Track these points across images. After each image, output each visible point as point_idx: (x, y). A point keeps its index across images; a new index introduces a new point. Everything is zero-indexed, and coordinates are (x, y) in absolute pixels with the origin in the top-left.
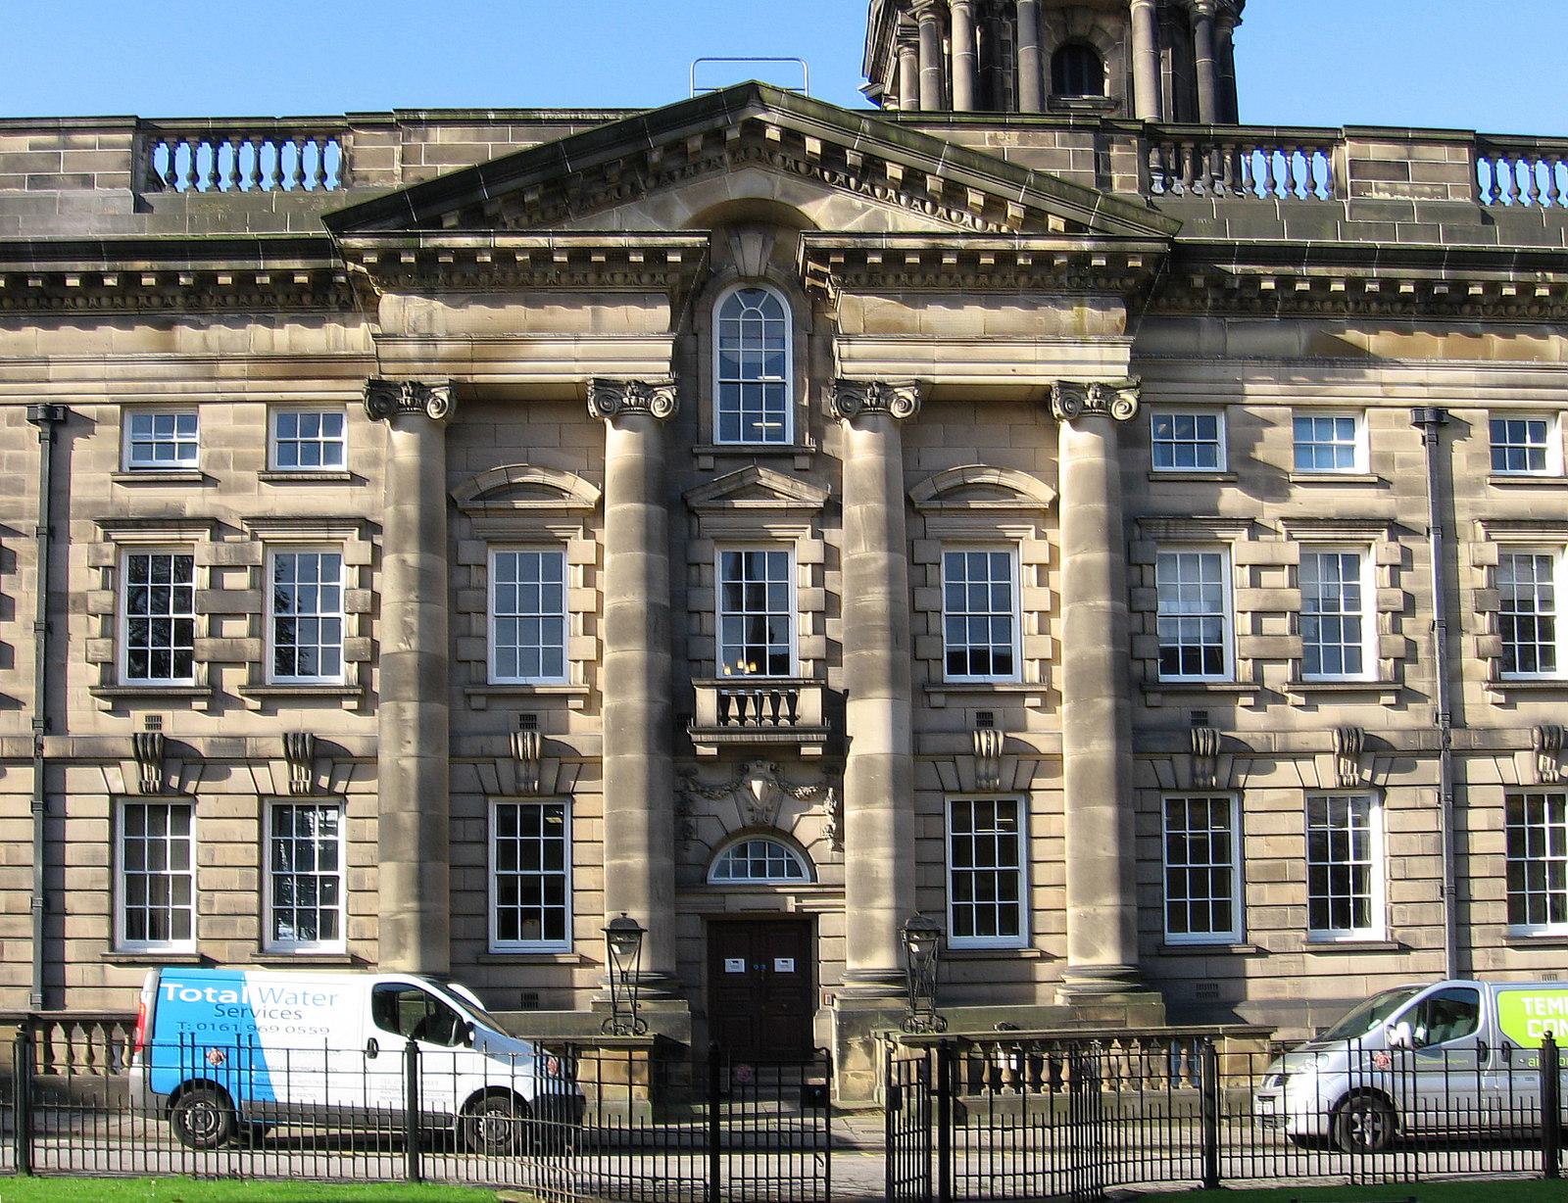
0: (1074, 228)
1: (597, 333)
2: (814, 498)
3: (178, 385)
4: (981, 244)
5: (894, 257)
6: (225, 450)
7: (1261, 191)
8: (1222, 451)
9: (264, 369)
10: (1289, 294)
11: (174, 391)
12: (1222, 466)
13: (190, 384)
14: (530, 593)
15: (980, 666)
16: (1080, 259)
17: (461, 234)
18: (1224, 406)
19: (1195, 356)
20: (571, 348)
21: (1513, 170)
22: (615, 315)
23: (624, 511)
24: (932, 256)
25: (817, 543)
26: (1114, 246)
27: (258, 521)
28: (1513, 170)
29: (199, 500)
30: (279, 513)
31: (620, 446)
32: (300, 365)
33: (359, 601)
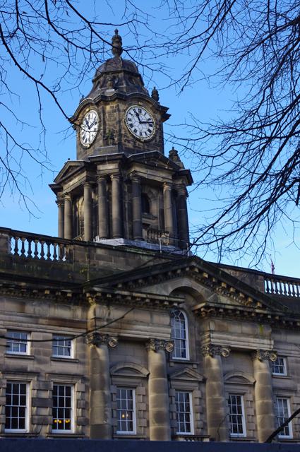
0: (264, 307)
1: (151, 323)
2: (200, 379)
3: (26, 325)
4: (246, 309)
5: (226, 310)
6: (40, 348)
7: (13, 252)
8: (285, 370)
9: (53, 322)
10: (134, 301)
11: (25, 327)
12: (28, 353)
13: (30, 325)
14: (61, 400)
15: (61, 427)
16: (266, 315)
17: (125, 291)
18: (286, 357)
19: (137, 322)
20: (146, 328)
21: (49, 247)
22: (157, 318)
23: (156, 381)
24: (234, 311)
25: (199, 392)
26: (273, 313)
27: (52, 374)
28: (49, 247)
29: (32, 366)
30: (57, 372)
31: (155, 358)
32: (62, 322)
33: (82, 404)
